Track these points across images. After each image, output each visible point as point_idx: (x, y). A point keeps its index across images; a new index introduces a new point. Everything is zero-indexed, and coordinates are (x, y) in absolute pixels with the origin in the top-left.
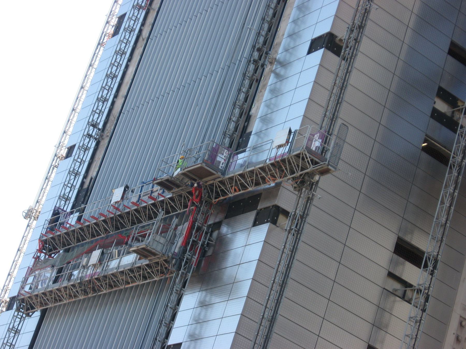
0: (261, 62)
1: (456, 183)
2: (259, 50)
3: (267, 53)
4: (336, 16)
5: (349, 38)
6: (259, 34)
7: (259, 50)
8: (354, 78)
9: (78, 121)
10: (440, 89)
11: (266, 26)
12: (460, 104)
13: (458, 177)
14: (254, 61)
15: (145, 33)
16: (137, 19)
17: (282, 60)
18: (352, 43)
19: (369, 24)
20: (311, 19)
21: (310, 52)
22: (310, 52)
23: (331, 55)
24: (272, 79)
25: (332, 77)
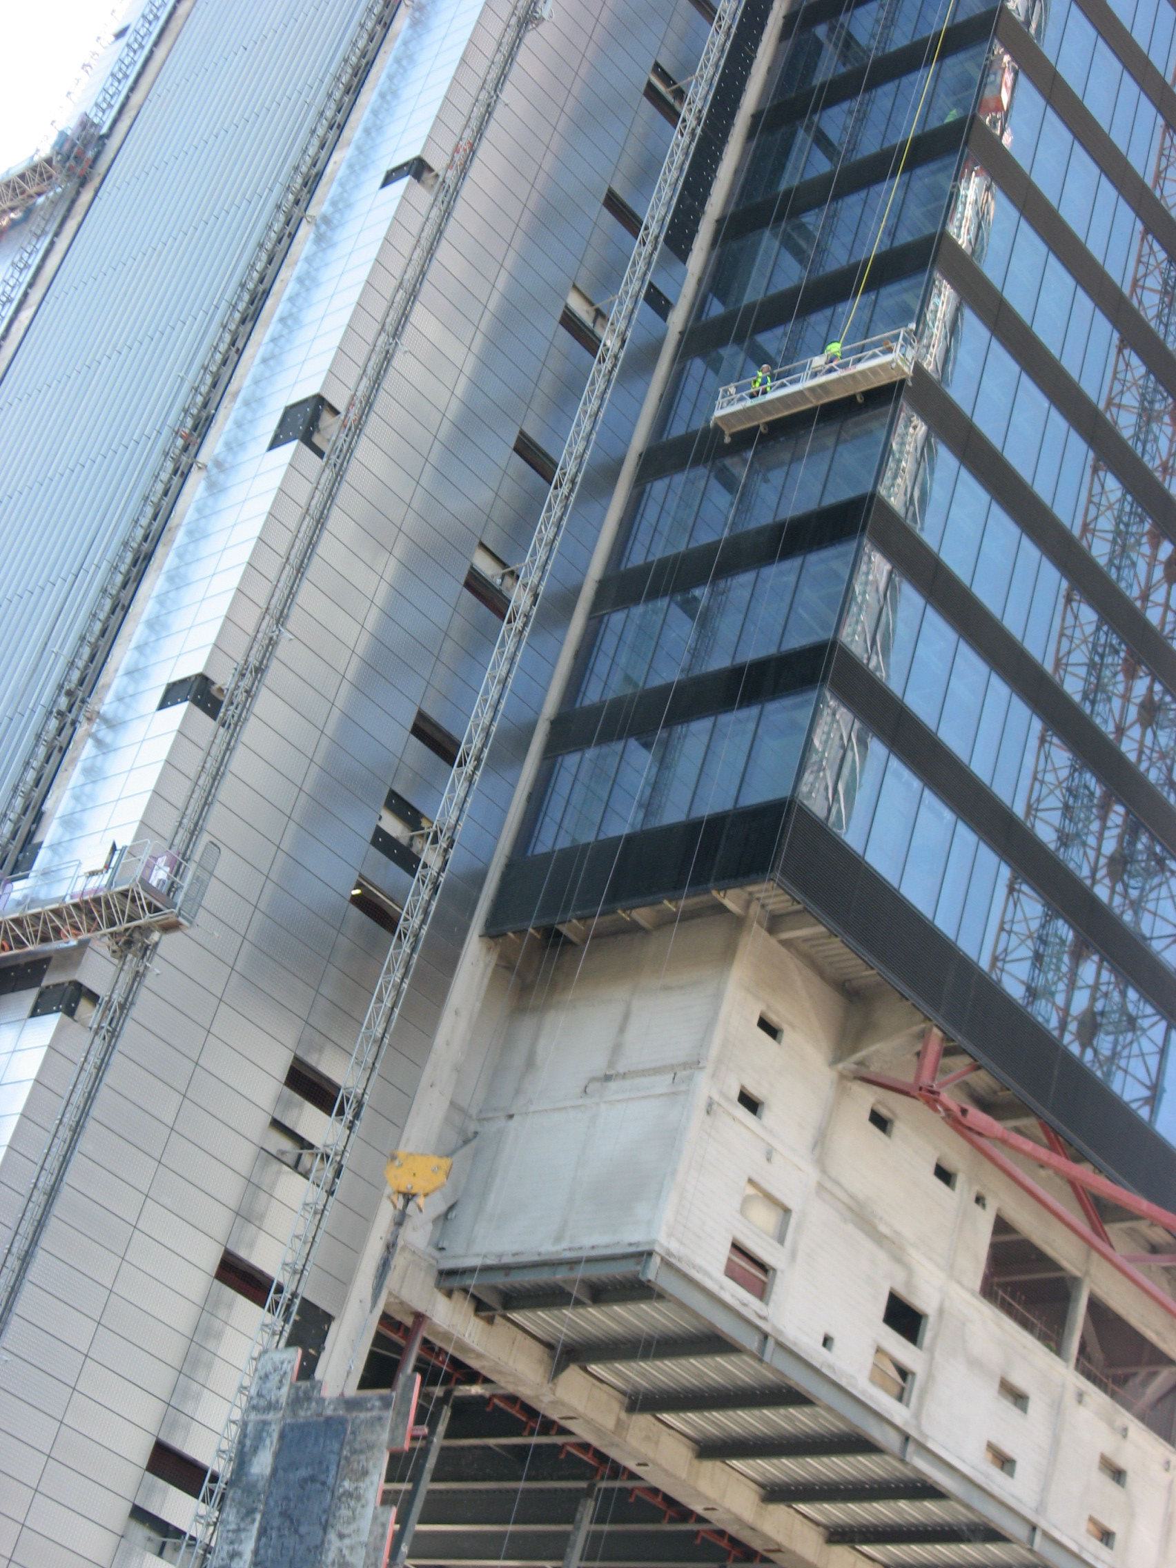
0: (71, 717)
1: (478, 759)
2: (70, 693)
3: (83, 701)
5: (237, 687)
6: (72, 664)
7: (70, 693)
8: (239, 761)
10: (393, 794)
12: (424, 823)
13: (481, 751)
14: (60, 713)
17: (110, 715)
18: (241, 697)
19: (274, 665)
20: (170, 647)
21: (162, 706)
22: (162, 706)
23: (199, 714)
24: (88, 749)
25: (200, 755)
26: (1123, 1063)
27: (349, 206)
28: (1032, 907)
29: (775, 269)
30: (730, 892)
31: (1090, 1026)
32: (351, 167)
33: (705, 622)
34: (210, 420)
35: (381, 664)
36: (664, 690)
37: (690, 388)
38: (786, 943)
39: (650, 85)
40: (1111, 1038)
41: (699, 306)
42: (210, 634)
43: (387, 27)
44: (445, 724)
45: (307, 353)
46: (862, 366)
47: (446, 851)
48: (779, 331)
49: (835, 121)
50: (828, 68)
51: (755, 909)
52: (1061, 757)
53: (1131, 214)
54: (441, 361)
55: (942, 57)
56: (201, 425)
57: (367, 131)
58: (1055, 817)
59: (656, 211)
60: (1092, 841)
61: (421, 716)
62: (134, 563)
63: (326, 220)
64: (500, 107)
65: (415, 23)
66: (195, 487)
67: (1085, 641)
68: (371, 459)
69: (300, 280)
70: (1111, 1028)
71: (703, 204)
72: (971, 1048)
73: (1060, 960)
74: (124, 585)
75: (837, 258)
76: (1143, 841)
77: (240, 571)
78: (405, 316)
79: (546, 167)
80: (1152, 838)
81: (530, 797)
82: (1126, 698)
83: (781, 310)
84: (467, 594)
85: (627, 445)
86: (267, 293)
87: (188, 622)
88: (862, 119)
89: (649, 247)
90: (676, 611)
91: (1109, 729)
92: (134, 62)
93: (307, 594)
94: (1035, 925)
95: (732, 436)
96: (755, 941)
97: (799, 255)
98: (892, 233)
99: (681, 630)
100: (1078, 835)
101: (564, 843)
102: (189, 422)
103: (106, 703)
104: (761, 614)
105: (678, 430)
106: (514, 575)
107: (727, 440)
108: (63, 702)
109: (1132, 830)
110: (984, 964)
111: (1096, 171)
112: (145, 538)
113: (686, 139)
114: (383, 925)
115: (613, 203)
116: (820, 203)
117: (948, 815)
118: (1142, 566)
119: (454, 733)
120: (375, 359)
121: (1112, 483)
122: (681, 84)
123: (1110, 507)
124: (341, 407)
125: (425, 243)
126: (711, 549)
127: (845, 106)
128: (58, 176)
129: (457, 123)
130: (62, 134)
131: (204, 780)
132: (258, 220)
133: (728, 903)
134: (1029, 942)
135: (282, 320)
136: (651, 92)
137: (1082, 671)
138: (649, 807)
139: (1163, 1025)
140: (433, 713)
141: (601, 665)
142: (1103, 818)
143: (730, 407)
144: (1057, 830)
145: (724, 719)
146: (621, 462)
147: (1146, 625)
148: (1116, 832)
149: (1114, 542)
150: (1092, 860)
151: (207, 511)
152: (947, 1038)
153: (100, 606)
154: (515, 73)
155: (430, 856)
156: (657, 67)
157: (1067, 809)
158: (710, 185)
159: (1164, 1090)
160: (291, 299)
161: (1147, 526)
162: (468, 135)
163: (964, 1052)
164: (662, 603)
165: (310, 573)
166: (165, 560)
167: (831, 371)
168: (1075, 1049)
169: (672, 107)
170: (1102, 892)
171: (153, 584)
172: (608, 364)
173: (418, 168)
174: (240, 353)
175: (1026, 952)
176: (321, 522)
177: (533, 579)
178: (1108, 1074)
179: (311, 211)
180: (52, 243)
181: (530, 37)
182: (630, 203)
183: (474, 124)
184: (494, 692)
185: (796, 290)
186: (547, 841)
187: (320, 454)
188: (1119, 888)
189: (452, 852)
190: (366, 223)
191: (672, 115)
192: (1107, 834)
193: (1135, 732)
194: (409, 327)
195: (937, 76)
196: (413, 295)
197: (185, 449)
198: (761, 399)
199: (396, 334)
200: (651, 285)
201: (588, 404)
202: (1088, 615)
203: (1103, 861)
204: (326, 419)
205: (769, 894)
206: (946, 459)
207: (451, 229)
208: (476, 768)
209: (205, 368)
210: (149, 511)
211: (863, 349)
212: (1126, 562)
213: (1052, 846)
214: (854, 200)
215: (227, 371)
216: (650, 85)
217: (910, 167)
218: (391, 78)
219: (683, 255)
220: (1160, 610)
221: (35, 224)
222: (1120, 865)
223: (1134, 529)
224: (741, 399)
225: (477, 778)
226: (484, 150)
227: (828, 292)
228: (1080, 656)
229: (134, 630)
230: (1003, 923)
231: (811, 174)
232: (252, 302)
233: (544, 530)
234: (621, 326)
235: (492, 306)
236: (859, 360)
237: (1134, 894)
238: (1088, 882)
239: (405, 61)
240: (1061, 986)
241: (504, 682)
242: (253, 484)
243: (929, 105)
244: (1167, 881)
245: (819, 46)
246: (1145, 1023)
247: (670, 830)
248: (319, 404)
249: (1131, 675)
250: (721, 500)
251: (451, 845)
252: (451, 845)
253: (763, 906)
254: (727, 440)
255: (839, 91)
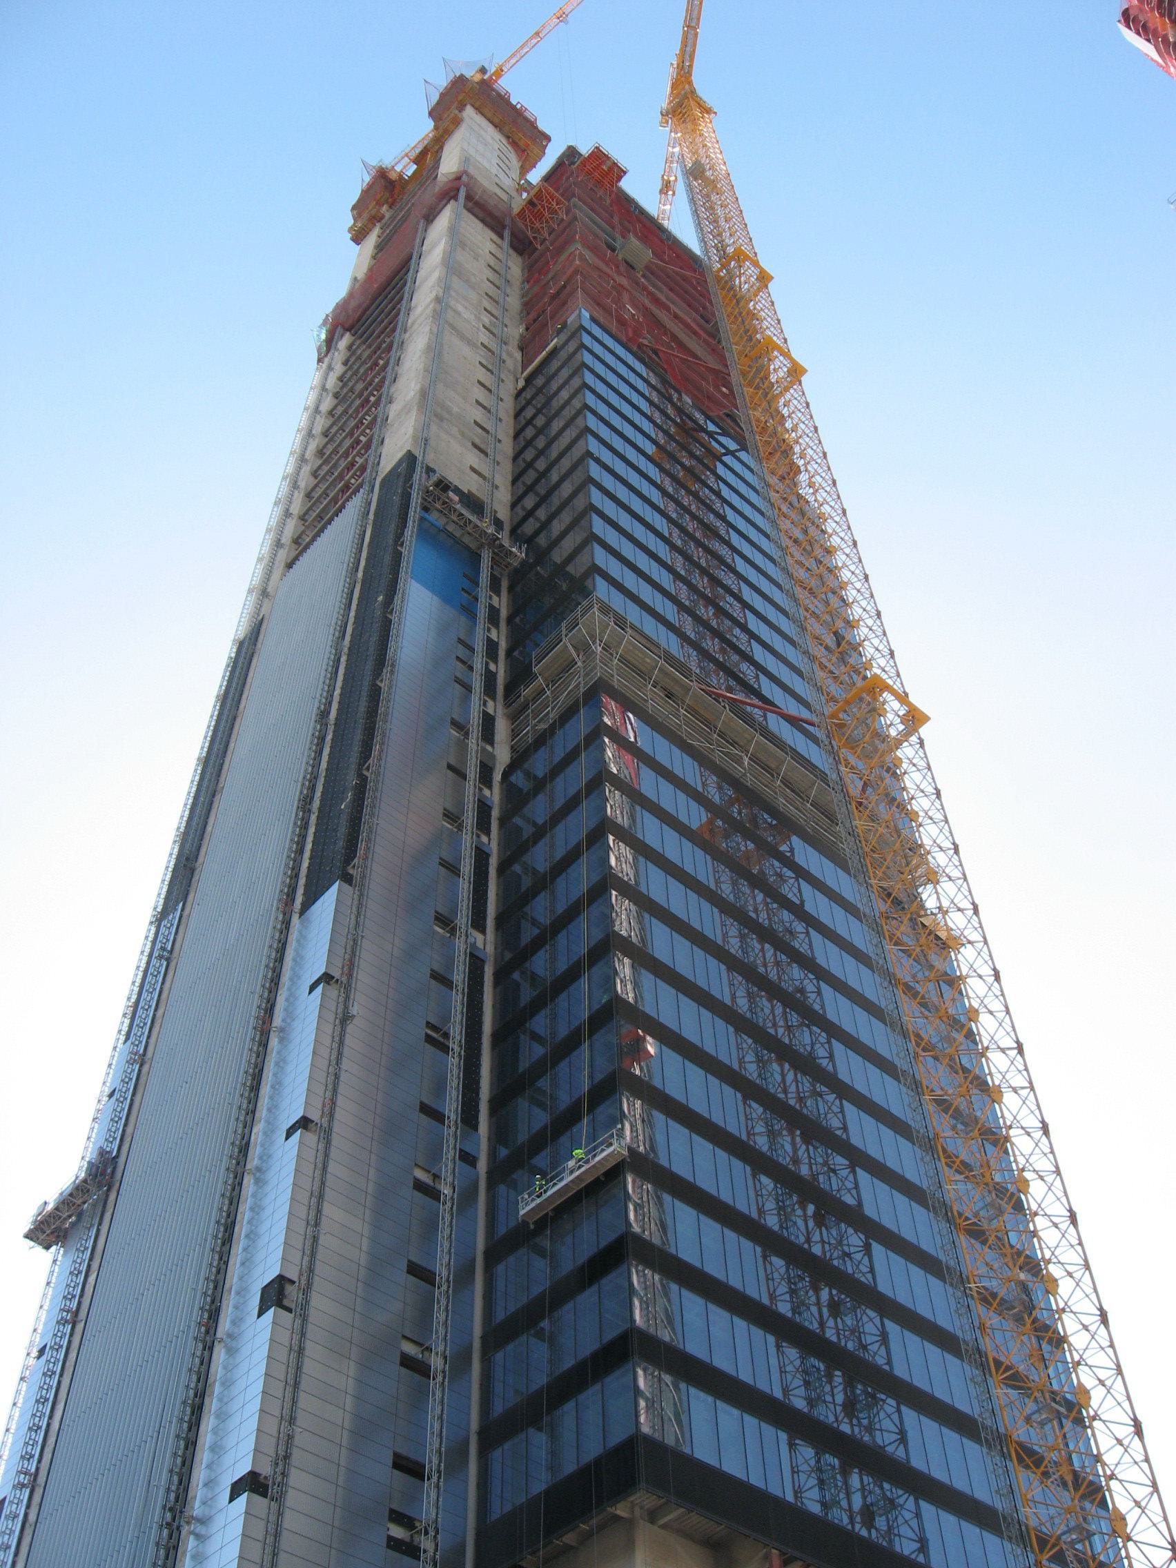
0: (175, 1524)
1: (439, 1472)
2: (171, 1509)
3: (181, 1512)
4: (244, 1535)
5: (275, 1473)
6: (168, 1490)
7: (171, 1509)
8: (290, 1521)
9: (13, 1444)
10: (392, 1511)
11: (176, 1478)
12: (417, 1524)
13: (439, 1466)
14: (167, 1524)
15: (32, 1517)
16: (20, 1501)
17: (200, 1516)
18: (279, 1479)
19: (295, 1452)
20: (228, 1459)
21: (231, 1500)
22: (231, 1500)
23: (257, 1498)
24: (192, 1542)
25: (263, 1524)
26: (877, 1426)
27: (270, 1156)
28: (807, 1452)
29: (531, 1118)
30: (619, 1505)
31: (868, 1515)
32: (265, 1133)
33: (552, 1341)
34: (218, 1310)
35: (363, 1430)
36: (539, 1392)
37: (502, 1203)
38: (664, 1527)
39: (427, 1035)
40: (884, 1518)
41: (492, 1154)
42: (250, 1443)
43: (266, 1046)
44: (412, 1456)
45: (267, 1253)
46: (597, 1159)
47: (435, 1537)
48: (543, 1153)
49: (540, 1023)
50: (527, 994)
51: (637, 1511)
52: (792, 1353)
53: (732, 1091)
54: (348, 1233)
55: (590, 1036)
56: (213, 1314)
57: (269, 1110)
58: (802, 1391)
59: (451, 1106)
60: (829, 1398)
61: (396, 1455)
62: (193, 1413)
63: (258, 1169)
64: (343, 1073)
65: (282, 1040)
66: (220, 1354)
67: (782, 1279)
68: (321, 1304)
69: (252, 1209)
70: (881, 1512)
71: (478, 1094)
72: (798, 1554)
73: (835, 1479)
74: (190, 1429)
75: (565, 1100)
76: (859, 1388)
77: (267, 1346)
78: (319, 1211)
79: (351, 1374)
80: (865, 1385)
81: (478, 1485)
82: (818, 1304)
83: (540, 1142)
84: (403, 1370)
85: (471, 1335)
86: (234, 1223)
87: (236, 1443)
88: (554, 1017)
89: (453, 1129)
90: (533, 1340)
91: (815, 1326)
92: (123, 1109)
93: (304, 1401)
94: (813, 1462)
95: (535, 1223)
96: (645, 1533)
97: (542, 1105)
98: (591, 1077)
99: (540, 1351)
100: (819, 1397)
101: (508, 1508)
102: (206, 1315)
103: (197, 1509)
104: (582, 1329)
105: (502, 1230)
106: (429, 1349)
107: (532, 1227)
108: (169, 1515)
109: (849, 1383)
110: (790, 1497)
111: (683, 887)
112: (196, 1396)
113: (460, 996)
114: (441, 1050)
115: (425, 1109)
116: (545, 1073)
117: (736, 1412)
118: (800, 1223)
119: (420, 1460)
120: (308, 1243)
121: (764, 1179)
122: (445, 1029)
123: (770, 1194)
124: (295, 1279)
125: (320, 1166)
126: (542, 1296)
127: (543, 1013)
128: (93, 1189)
129: (320, 1090)
130: (89, 1162)
131: (270, 1539)
132: (218, 1180)
133: (618, 1512)
134: (813, 1475)
135: (247, 1236)
136: (429, 1039)
137: (787, 1297)
138: (553, 1468)
139: (912, 1498)
140: (403, 1451)
141: (498, 1387)
142: (830, 1382)
143: (527, 1206)
144: (805, 1399)
145: (581, 1397)
146: (474, 1260)
147: (815, 1256)
148: (841, 1388)
149: (779, 1214)
150: (817, 1316)
151: (225, 1400)
152: (782, 1553)
153: (178, 1447)
154: (346, 1051)
155: (426, 1544)
156: (428, 1024)
157: (807, 1384)
158: (478, 1082)
159: (927, 1540)
160: (249, 1222)
161: (795, 1199)
162: (329, 1094)
163: (796, 1559)
164: (523, 1338)
165: (303, 1386)
166: (212, 1405)
167: (580, 1167)
168: (864, 1533)
169: (443, 1044)
170: (845, 1428)
171: (208, 1423)
172: (449, 1204)
173: (304, 1123)
174: (226, 1263)
175: (813, 1482)
176: (301, 1351)
177: (441, 1348)
178: (891, 1542)
179: (248, 1166)
180: (98, 1231)
181: (350, 1028)
182: (434, 1106)
183: (330, 1087)
184: (437, 1426)
185: (545, 1127)
186: (497, 1510)
187: (290, 1310)
188: (855, 1421)
189: (439, 1537)
190: (282, 1163)
191: (445, 1049)
192: (836, 1391)
193: (831, 1323)
194: (323, 1218)
195: (591, 1046)
196: (321, 1197)
197: (207, 1332)
198: (544, 1197)
199: (317, 1224)
200: (461, 1150)
201: (444, 1232)
202: (778, 1262)
203: (839, 1409)
204: (289, 1289)
205: (642, 1499)
206: (659, 1117)
207: (333, 1153)
208: (439, 1478)
209: (207, 1279)
210: (194, 1377)
211: (595, 1148)
212: (789, 1224)
213: (806, 1410)
214: (564, 1065)
215: (221, 1277)
216: (427, 1035)
217: (591, 1109)
218: (275, 1075)
219: (475, 1127)
220: (819, 1245)
221: (85, 1218)
222: (850, 1407)
223: (788, 1203)
224: (533, 1200)
225: (441, 1484)
226: (340, 1101)
227: (566, 1121)
228: (783, 1288)
229: (203, 1456)
230: (767, 1276)
231: (537, 1127)
232: (226, 1231)
233: (439, 1316)
234: (450, 1179)
235: (370, 1190)
236: (595, 1156)
237: (865, 1422)
238: (835, 1425)
239: (281, 1063)
240: (842, 1496)
241: (441, 1417)
242: (255, 1340)
243: (591, 1066)
244: (882, 1408)
245: (518, 985)
246: (901, 1501)
247: (570, 1478)
248: (281, 1281)
249: (817, 1291)
250: (540, 1264)
251: (437, 1532)
252: (437, 1532)
253: (642, 1508)
254: (532, 1227)
255: (537, 1005)
